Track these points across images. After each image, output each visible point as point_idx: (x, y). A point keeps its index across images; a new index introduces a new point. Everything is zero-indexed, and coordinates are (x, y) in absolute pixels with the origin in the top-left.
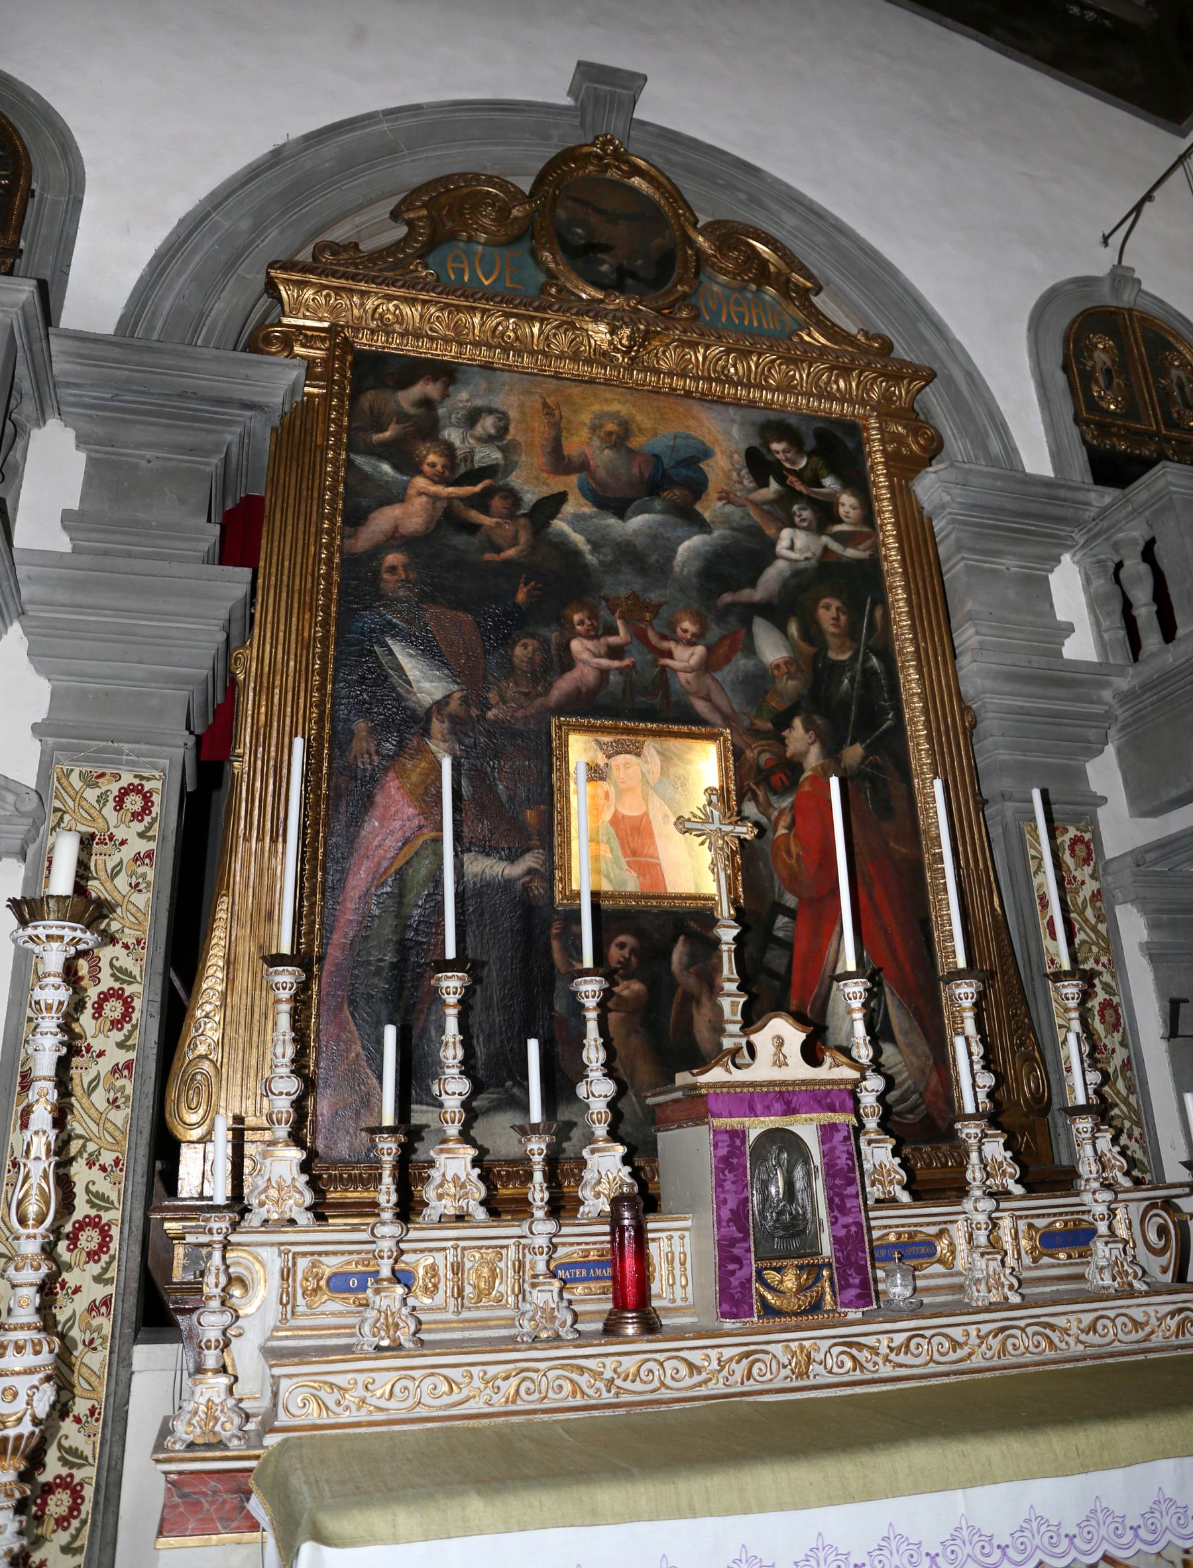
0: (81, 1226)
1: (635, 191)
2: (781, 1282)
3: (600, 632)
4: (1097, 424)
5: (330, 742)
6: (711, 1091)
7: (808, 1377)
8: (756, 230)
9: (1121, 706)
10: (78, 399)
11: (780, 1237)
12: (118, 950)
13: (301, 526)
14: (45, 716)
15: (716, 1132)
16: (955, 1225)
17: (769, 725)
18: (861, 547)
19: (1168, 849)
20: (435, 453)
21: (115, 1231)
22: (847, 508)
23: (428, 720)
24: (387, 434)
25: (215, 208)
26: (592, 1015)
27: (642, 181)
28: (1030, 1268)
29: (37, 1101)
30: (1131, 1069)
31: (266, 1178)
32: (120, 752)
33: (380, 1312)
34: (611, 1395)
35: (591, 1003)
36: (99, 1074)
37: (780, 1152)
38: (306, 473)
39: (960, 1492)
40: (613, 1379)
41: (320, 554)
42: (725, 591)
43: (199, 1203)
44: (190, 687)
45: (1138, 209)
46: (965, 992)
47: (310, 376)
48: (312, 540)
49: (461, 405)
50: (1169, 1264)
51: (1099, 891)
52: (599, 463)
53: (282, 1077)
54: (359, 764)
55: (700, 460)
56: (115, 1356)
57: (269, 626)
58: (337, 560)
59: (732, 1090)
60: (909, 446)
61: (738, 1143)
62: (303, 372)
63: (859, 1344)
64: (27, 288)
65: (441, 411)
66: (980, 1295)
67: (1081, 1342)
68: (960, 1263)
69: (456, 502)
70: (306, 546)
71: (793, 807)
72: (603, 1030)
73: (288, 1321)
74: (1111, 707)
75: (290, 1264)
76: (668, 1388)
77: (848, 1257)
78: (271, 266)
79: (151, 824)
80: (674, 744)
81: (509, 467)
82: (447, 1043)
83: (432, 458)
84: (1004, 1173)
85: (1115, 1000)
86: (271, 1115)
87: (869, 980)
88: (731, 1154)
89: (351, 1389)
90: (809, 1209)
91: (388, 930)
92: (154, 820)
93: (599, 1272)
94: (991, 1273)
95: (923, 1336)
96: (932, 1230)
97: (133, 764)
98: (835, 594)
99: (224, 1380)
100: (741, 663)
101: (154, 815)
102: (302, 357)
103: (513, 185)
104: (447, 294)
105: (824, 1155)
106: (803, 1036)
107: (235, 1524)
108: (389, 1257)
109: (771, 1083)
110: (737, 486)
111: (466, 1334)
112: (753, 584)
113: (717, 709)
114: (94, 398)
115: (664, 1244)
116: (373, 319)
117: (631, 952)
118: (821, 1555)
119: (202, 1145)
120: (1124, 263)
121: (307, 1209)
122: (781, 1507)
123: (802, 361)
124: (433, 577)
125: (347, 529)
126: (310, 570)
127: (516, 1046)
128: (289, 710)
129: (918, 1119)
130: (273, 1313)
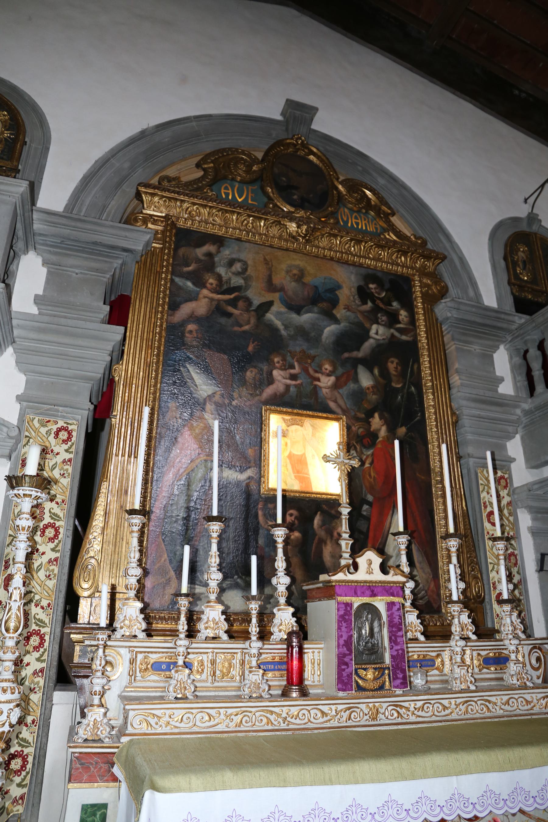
0: (46, 527)
1: (311, 162)
2: (366, 675)
3: (287, 367)
4: (518, 286)
6: (337, 584)
7: (377, 720)
8: (366, 184)
9: (524, 417)
10: (44, 242)
11: (366, 654)
12: (53, 504)
13: (148, 309)
14: (22, 392)
17: (363, 416)
18: (409, 335)
19: (544, 484)
20: (212, 278)
21: (47, 638)
22: (403, 317)
23: (205, 404)
24: (190, 268)
25: (113, 156)
26: (280, 546)
28: (478, 674)
29: (16, 573)
30: (521, 585)
31: (124, 615)
32: (58, 411)
33: (177, 681)
34: (285, 725)
36: (42, 563)
37: (368, 614)
38: (151, 284)
39: (455, 777)
40: (286, 717)
41: (157, 322)
42: (345, 352)
43: (88, 626)
45: (542, 186)
46: (453, 544)
48: (153, 316)
49: (226, 257)
50: (541, 675)
51: (510, 502)
53: (133, 568)
55: (336, 290)
56: (45, 696)
57: (131, 355)
59: (347, 584)
60: (432, 290)
61: (349, 609)
62: (153, 235)
63: (401, 705)
64: (24, 185)
65: (216, 259)
66: (457, 685)
67: (502, 709)
68: (447, 669)
69: (222, 302)
70: (150, 318)
71: (373, 454)
73: (132, 683)
74: (520, 417)
75: (134, 657)
76: (312, 722)
77: (397, 665)
79: (71, 446)
81: (247, 287)
82: (212, 556)
83: (211, 281)
85: (516, 552)
86: (127, 585)
87: (409, 536)
88: (345, 614)
89: (163, 717)
90: (380, 642)
91: (182, 502)
92: (73, 444)
93: (279, 667)
94: (462, 675)
95: (430, 703)
96: (434, 654)
97: (63, 417)
99: (103, 710)
100: (352, 386)
101: (73, 441)
103: (254, 156)
107: (106, 778)
108: (183, 656)
109: (365, 582)
110: (353, 303)
111: (217, 694)
112: (358, 349)
113: (340, 406)
114: (52, 242)
118: (390, 804)
119: (90, 599)
120: (534, 211)
121: (143, 631)
122: (373, 781)
123: (385, 247)
125: (170, 311)
127: (240, 559)
128: (139, 395)
129: (424, 603)
130: (125, 680)
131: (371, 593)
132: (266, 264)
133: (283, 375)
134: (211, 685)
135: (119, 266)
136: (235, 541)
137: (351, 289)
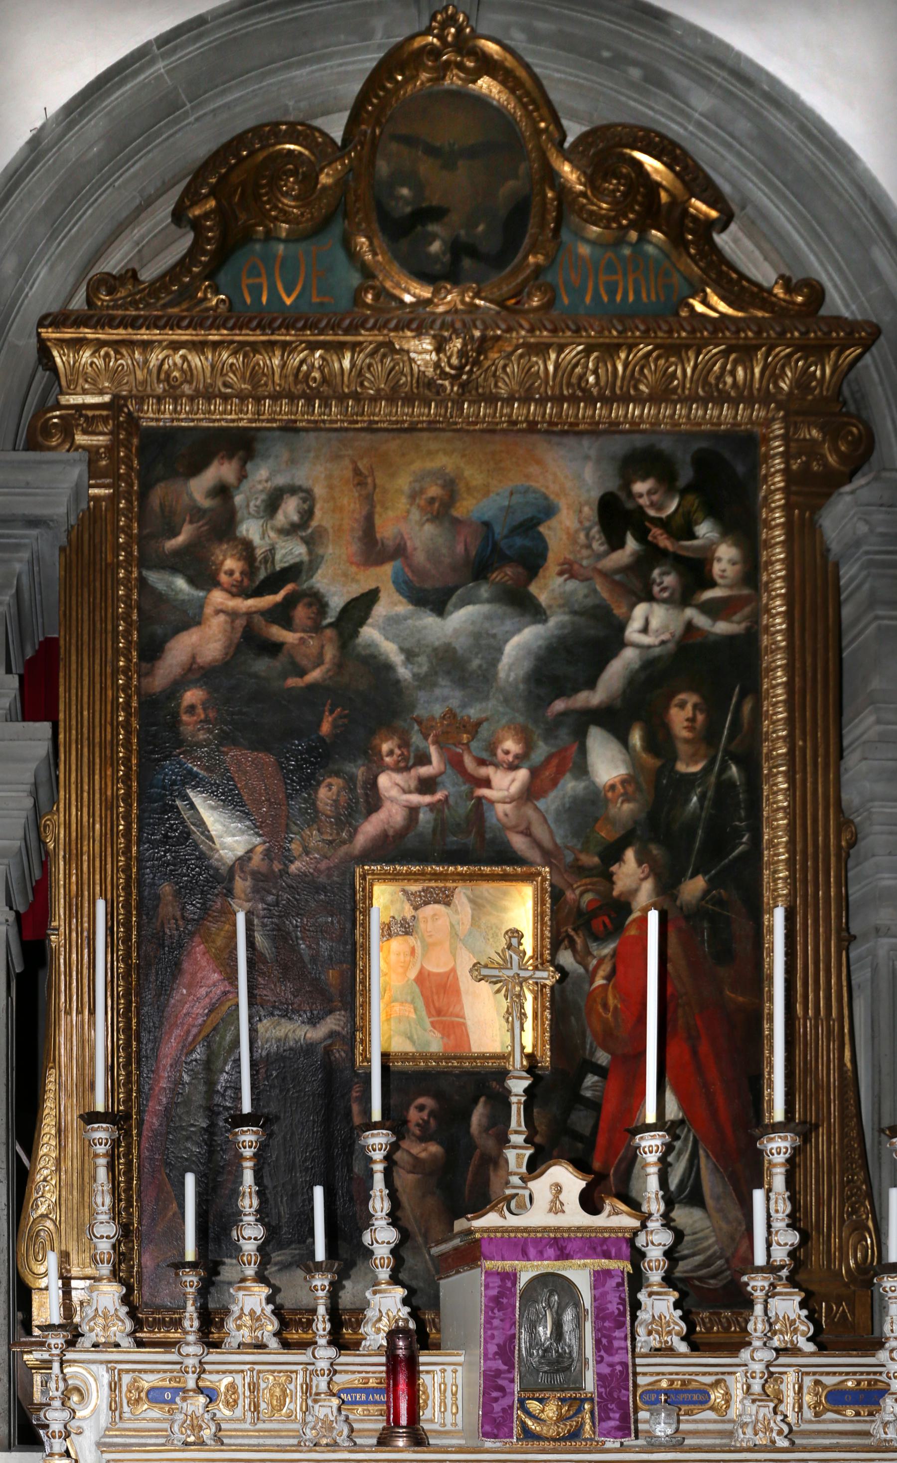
1: (481, 102)
2: (543, 1411)
3: (411, 763)
5: (137, 909)
6: (485, 1235)
13: (97, 668)
15: (488, 1274)
16: (733, 1377)
17: (596, 860)
18: (737, 618)
20: (232, 556)
23: (231, 879)
24: (181, 539)
26: (379, 1167)
27: (493, 83)
28: (811, 1422)
35: (378, 1155)
37: (551, 1295)
38: (98, 601)
41: (118, 698)
42: (557, 697)
44: (6, 861)
47: (94, 472)
48: (109, 682)
49: (260, 487)
52: (418, 544)
54: (167, 931)
55: (539, 523)
57: (73, 786)
58: (134, 704)
59: (506, 1235)
60: (823, 457)
62: (84, 467)
66: (745, 1437)
70: (104, 689)
71: (615, 954)
72: (389, 1182)
77: (610, 1394)
78: (40, 324)
80: (486, 888)
84: (795, 1331)
86: (95, 1255)
88: (501, 1295)
90: (575, 1349)
93: (377, 1397)
94: (761, 1417)
96: (709, 1380)
98: (692, 688)
100: (570, 786)
102: (84, 448)
104: (241, 329)
105: (595, 1299)
106: (583, 1184)
109: (545, 1229)
110: (585, 552)
113: (537, 844)
115: (438, 1378)
116: (159, 381)
117: (429, 1115)
123: (688, 347)
124: (233, 714)
125: (144, 665)
126: (109, 719)
128: (97, 877)
129: (721, 1284)
131: (559, 1253)
132: (359, 484)
133: (402, 783)
134: (251, 1428)
135: (25, 568)
136: (307, 1169)
137: (580, 511)
